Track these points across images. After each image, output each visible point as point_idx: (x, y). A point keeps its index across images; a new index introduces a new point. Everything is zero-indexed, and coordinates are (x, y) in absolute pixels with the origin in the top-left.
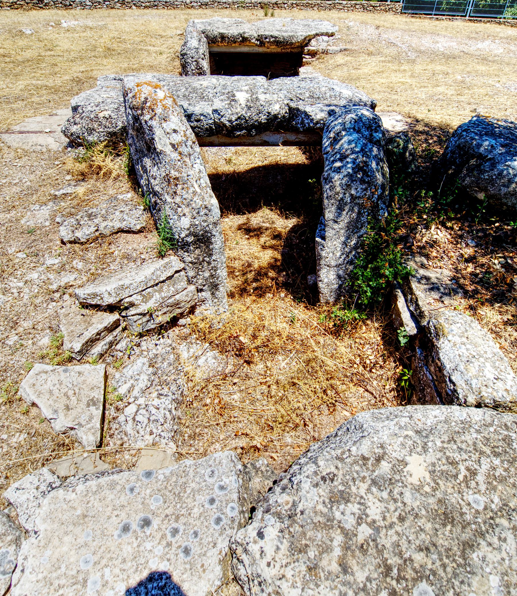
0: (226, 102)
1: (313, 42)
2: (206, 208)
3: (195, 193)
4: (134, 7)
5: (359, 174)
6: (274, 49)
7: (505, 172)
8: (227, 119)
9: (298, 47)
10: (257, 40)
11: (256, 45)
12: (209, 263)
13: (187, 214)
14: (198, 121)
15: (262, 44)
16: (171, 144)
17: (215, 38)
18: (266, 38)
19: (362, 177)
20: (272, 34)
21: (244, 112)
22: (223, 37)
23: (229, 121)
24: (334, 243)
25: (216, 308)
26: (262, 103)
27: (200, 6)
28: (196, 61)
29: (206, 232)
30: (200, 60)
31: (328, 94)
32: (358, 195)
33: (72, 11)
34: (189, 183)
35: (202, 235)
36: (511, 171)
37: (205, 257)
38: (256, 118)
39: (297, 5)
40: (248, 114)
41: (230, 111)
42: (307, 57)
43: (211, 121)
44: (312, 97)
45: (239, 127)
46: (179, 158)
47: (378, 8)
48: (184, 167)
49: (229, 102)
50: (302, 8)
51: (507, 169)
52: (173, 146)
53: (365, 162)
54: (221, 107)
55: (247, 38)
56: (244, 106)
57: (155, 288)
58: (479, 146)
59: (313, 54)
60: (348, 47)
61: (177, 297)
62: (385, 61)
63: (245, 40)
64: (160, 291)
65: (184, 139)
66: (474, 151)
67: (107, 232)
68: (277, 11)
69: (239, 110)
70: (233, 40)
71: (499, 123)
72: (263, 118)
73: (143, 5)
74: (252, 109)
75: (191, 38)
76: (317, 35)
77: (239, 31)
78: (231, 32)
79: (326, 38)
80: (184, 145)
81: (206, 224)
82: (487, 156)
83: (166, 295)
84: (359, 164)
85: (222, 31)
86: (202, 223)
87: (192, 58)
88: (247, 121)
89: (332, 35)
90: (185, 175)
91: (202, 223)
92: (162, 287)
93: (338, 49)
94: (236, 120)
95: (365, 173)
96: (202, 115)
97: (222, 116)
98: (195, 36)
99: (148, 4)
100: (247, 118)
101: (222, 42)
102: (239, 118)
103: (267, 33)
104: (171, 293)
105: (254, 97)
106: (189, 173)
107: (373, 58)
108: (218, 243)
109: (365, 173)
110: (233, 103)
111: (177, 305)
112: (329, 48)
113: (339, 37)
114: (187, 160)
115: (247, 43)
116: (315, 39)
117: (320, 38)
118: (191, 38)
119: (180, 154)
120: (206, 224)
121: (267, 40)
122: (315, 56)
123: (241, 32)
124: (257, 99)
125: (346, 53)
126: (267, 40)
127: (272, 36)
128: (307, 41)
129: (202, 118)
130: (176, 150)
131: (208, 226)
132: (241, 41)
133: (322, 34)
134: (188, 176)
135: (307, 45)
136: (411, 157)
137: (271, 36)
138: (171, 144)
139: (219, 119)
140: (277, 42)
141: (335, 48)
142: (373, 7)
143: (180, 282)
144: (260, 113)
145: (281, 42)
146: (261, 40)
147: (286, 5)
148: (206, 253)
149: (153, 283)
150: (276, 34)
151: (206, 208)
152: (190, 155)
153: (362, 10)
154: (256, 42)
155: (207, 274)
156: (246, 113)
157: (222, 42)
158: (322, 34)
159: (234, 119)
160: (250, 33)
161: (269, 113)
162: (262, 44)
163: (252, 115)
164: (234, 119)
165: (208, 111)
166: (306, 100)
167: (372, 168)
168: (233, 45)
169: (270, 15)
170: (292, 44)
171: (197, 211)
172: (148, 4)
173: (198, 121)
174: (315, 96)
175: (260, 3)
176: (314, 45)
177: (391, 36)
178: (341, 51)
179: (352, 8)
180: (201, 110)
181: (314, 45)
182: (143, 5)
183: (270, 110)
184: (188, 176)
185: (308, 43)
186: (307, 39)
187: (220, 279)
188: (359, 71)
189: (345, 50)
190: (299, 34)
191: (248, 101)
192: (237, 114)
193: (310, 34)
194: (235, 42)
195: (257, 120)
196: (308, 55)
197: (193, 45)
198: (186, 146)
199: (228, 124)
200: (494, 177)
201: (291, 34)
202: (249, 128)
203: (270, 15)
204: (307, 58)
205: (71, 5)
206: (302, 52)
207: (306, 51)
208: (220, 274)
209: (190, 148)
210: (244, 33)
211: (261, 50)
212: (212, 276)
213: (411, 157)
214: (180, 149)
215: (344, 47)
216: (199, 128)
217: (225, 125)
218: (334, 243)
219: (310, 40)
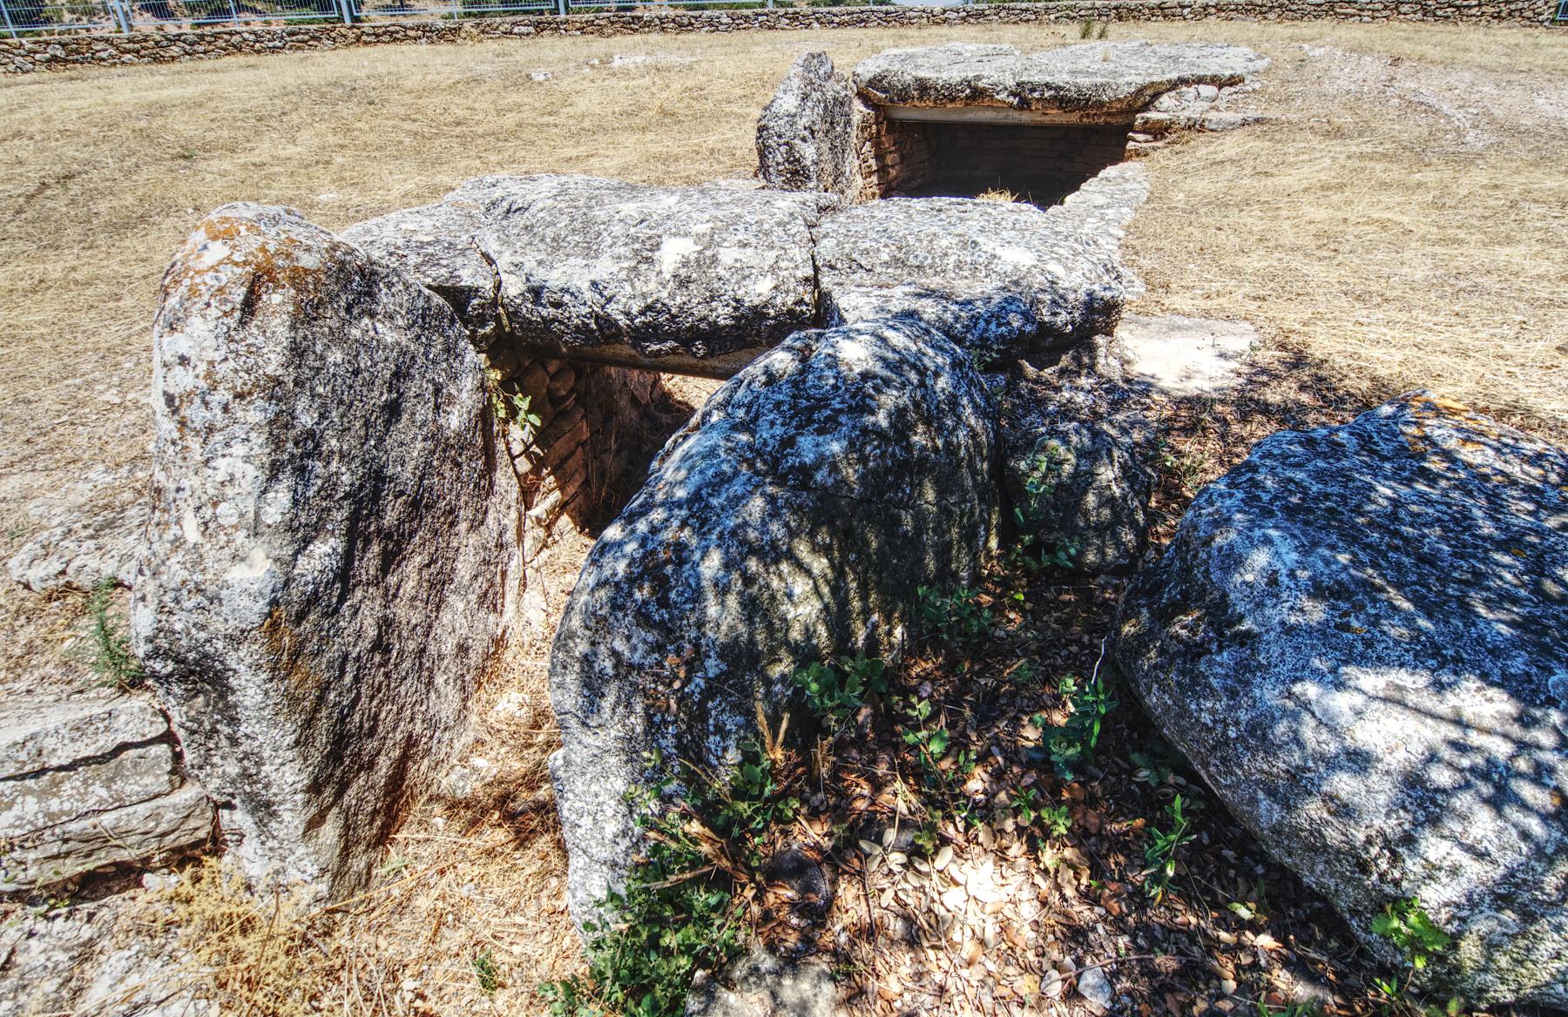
0: (626, 264)
1: (1166, 101)
2: (199, 590)
3: (177, 543)
4: (815, 25)
5: (641, 588)
6: (1055, 116)
7: (1281, 728)
8: (621, 307)
9: (1121, 112)
10: (1012, 94)
11: (1011, 106)
12: (234, 741)
13: (149, 598)
14: (557, 305)
15: (1024, 104)
16: (165, 393)
17: (906, 88)
18: (1033, 90)
19: (645, 603)
20: (1048, 79)
21: (665, 294)
22: (923, 87)
23: (627, 314)
24: (594, 788)
25: (277, 864)
26: (722, 272)
27: (963, 18)
28: (787, 144)
29: (206, 656)
30: (797, 141)
31: (953, 258)
32: (636, 658)
33: (692, 36)
34: (173, 512)
35: (197, 663)
36: (1308, 732)
37: (218, 722)
38: (701, 311)
39: (1221, 10)
40: (679, 300)
41: (628, 288)
42: (1140, 137)
43: (585, 310)
44: (898, 262)
45: (652, 332)
46: (176, 435)
47: (1474, 11)
48: (179, 462)
49: (633, 263)
50: (1233, 14)
51: (1295, 716)
52: (170, 399)
53: (680, 547)
54: (605, 277)
55: (986, 90)
56: (668, 277)
57: (30, 783)
58: (1232, 559)
59: (1158, 131)
60: (1271, 114)
61: (107, 820)
62: (1362, 156)
63: (977, 94)
64: (42, 795)
65: (203, 384)
66: (1207, 573)
67: (85, 581)
68: (1115, 28)
69: (652, 286)
70: (948, 94)
71: (1468, 454)
72: (722, 314)
73: (837, 20)
74: (692, 286)
75: (785, 92)
76: (1183, 81)
77: (963, 75)
78: (945, 76)
79: (1208, 90)
80: (197, 401)
81: (202, 635)
82: (1241, 618)
83: (66, 806)
84: (654, 552)
85: (922, 74)
86: (194, 631)
87: (780, 137)
88: (674, 317)
89: (1233, 81)
90: (173, 486)
91: (194, 631)
92: (56, 784)
93: (1239, 117)
94: (642, 313)
95: (661, 585)
96: (565, 290)
97: (609, 300)
98: (795, 87)
99: (846, 18)
100: (674, 311)
101: (921, 98)
102: (649, 308)
103: (1036, 79)
104: (91, 803)
105: (708, 253)
106: (185, 483)
107: (1336, 146)
108: (251, 692)
109: (661, 585)
110: (643, 267)
111: (100, 840)
112: (1213, 115)
113: (1257, 86)
114: (194, 444)
115: (987, 102)
116: (1173, 93)
117: (1190, 92)
118: (785, 92)
119: (183, 424)
120: (202, 635)
121: (1036, 95)
122: (1163, 137)
123: (971, 75)
124: (714, 260)
125: (1258, 128)
126: (1036, 95)
127: (1048, 86)
128: (1148, 96)
129: (567, 298)
130: (174, 412)
131: (209, 641)
132: (967, 97)
133: (1200, 80)
134: (178, 490)
135: (1146, 107)
136: (1106, 512)
137: (1047, 85)
138: (165, 393)
139: (603, 307)
140: (1062, 100)
141: (1230, 116)
142: (1458, 8)
143: (141, 774)
144: (712, 298)
145: (1070, 100)
146: (1023, 95)
147: (1186, 11)
148: (220, 712)
149: (12, 771)
150: (1060, 79)
151: (199, 590)
152: (211, 430)
153: (1419, 16)
154: (1011, 99)
155: (233, 769)
156: (672, 296)
157: (921, 98)
158: (1200, 80)
159: (635, 311)
160: (995, 79)
161: (737, 301)
162: (1024, 104)
163: (694, 305)
164: (635, 311)
165: (579, 283)
166: (878, 269)
167: (698, 578)
168: (949, 106)
169: (1095, 33)
170: (1101, 104)
171: (172, 595)
172: (846, 18)
173: (557, 305)
174: (912, 261)
175: (1116, 8)
176: (1166, 108)
177: (1428, 87)
178: (1245, 123)
179: (1385, 13)
180: (564, 279)
181: (1166, 108)
182: (837, 20)
183: (740, 293)
184: (178, 490)
185: (1151, 102)
186: (1150, 92)
187: (274, 790)
188: (1269, 181)
189: (1257, 121)
190: (1121, 81)
191: (685, 264)
192: (644, 296)
193: (1155, 79)
194: (953, 100)
195: (704, 319)
196: (1144, 132)
197: (785, 107)
198: (206, 404)
199: (623, 321)
200: (1232, 733)
201: (1099, 80)
202: (687, 337)
203: (1095, 33)
204: (1138, 141)
205: (691, 24)
206: (1130, 127)
207: (1138, 122)
208: (273, 776)
209: (218, 412)
210: (978, 78)
211: (1025, 117)
212: (245, 775)
213: (1106, 512)
214: (186, 412)
215: (1258, 115)
216: (561, 323)
217: (615, 323)
218: (594, 788)
219: (1157, 95)
